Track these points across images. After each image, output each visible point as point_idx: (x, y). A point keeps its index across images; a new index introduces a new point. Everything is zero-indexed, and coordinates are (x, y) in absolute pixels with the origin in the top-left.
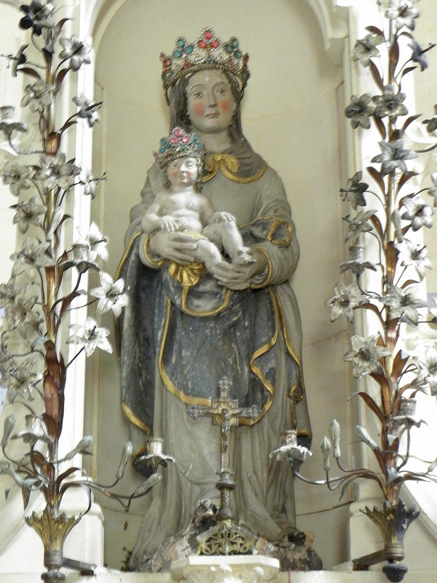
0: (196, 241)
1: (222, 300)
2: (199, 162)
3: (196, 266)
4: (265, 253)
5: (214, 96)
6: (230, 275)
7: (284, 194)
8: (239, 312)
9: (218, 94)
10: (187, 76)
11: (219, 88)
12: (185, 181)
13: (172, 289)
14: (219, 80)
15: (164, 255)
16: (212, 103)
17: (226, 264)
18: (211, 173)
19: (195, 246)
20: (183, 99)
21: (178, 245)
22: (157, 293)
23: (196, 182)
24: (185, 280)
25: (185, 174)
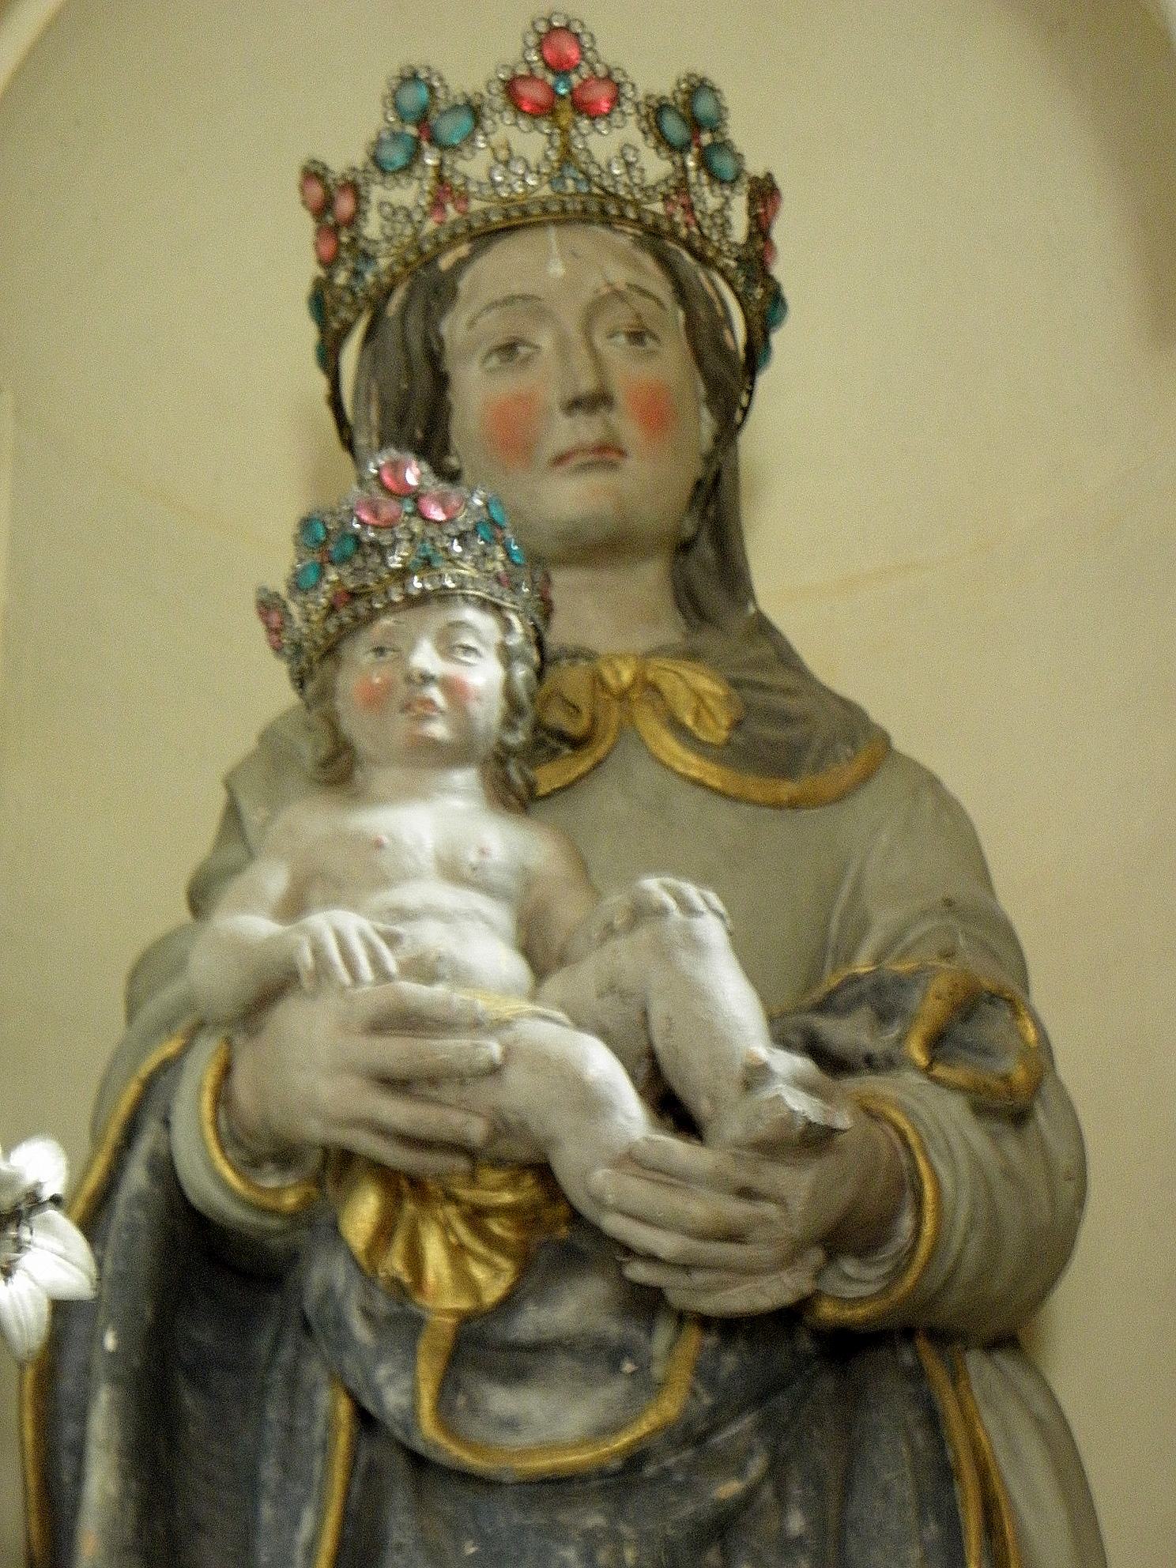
0: (502, 1025)
1: (647, 1386)
2: (516, 640)
3: (497, 1189)
4: (896, 1115)
5: (594, 353)
6: (701, 1208)
7: (984, 877)
8: (750, 1452)
9: (616, 351)
10: (445, 263)
11: (621, 316)
12: (438, 730)
13: (361, 1331)
14: (620, 276)
15: (314, 1130)
16: (587, 384)
17: (679, 1149)
18: (578, 743)
19: (493, 1049)
20: (424, 380)
21: (393, 1051)
22: (277, 1376)
23: (501, 744)
24: (438, 1276)
25: (435, 693)
